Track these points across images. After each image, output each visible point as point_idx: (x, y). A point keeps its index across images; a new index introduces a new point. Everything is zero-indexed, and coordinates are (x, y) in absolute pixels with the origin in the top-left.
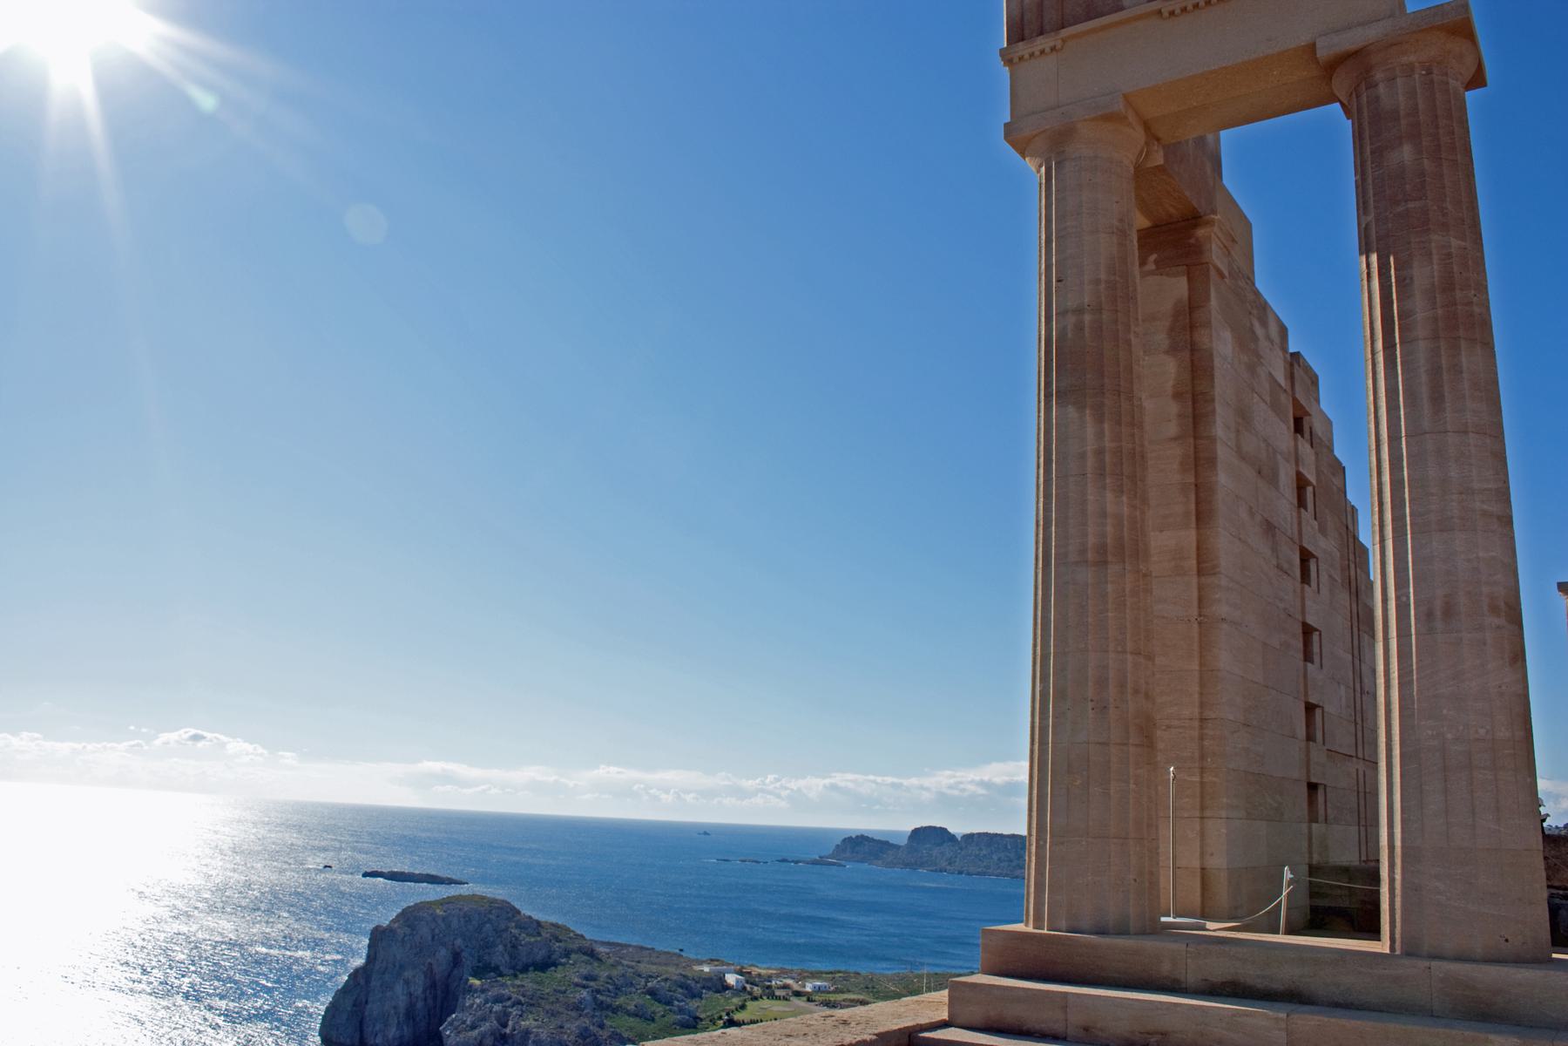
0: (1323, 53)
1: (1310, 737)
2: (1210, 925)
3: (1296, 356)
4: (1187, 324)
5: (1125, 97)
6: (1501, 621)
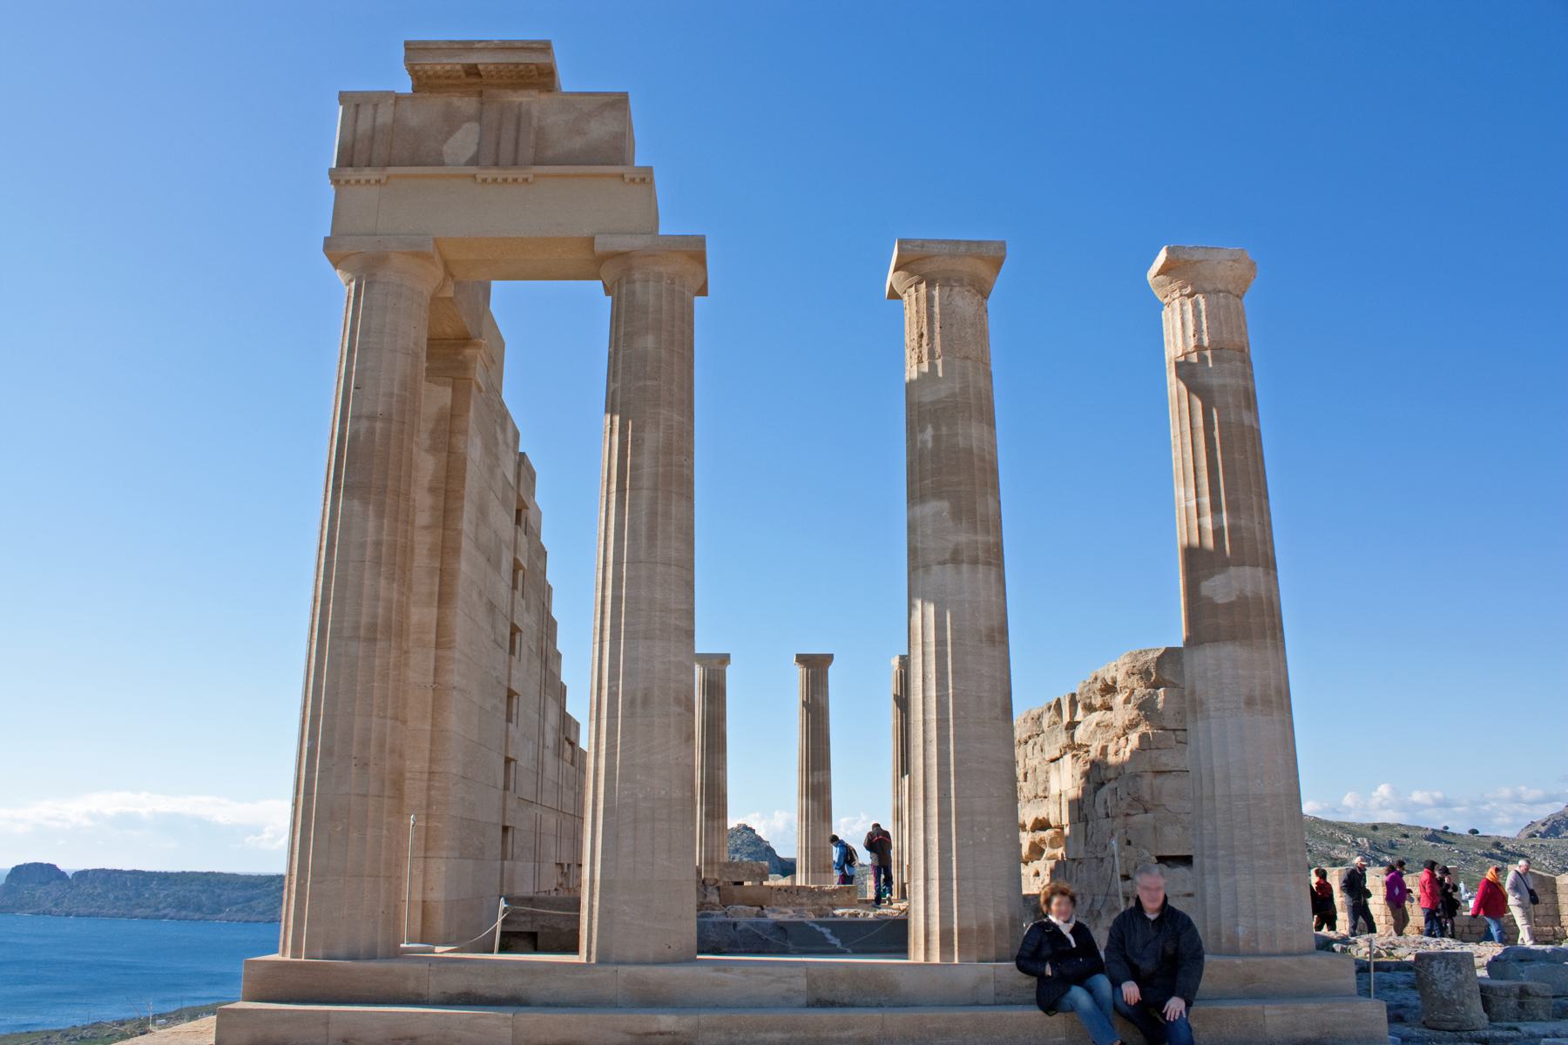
0: (598, 249)
1: (506, 788)
2: (438, 949)
3: (523, 455)
4: (448, 429)
5: (435, 240)
6: (682, 710)
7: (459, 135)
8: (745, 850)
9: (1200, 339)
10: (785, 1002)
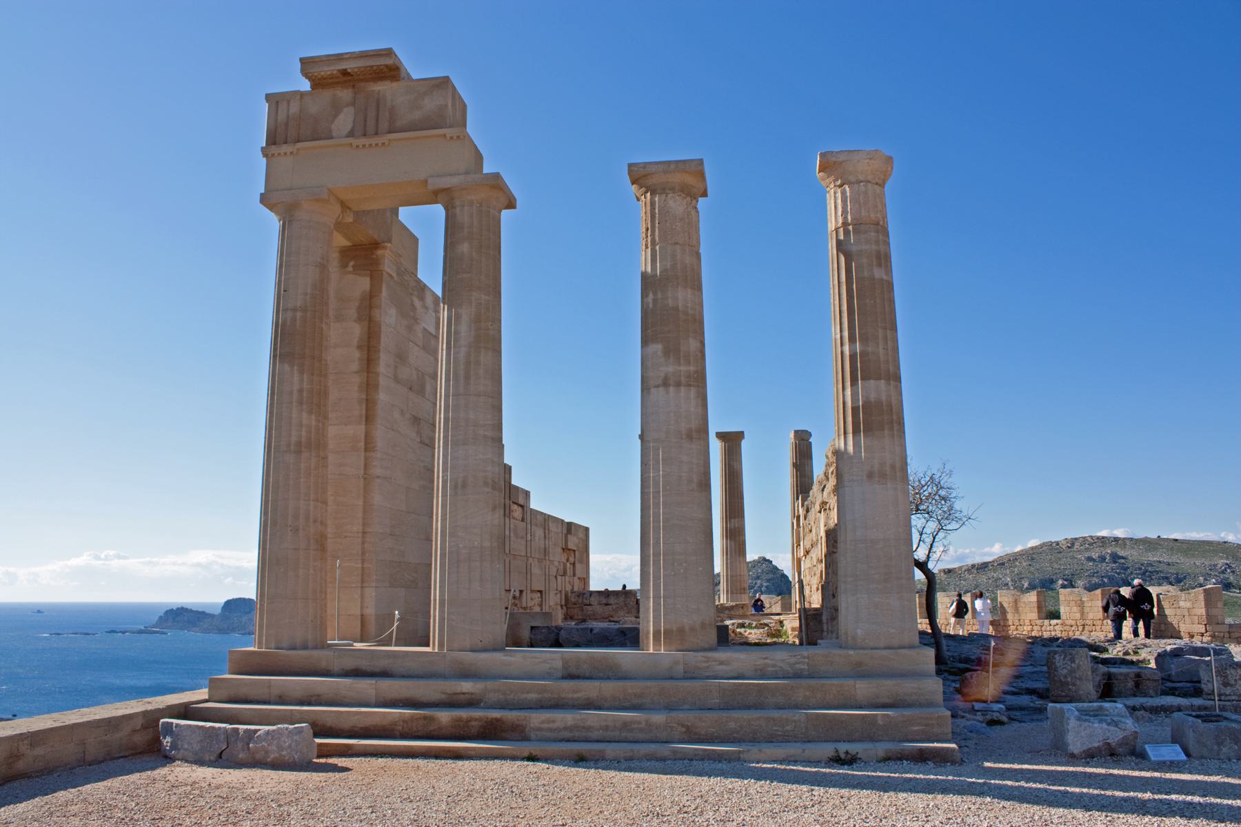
0: (430, 187)
7: (341, 116)
8: (765, 577)
9: (845, 218)
10: (547, 676)
